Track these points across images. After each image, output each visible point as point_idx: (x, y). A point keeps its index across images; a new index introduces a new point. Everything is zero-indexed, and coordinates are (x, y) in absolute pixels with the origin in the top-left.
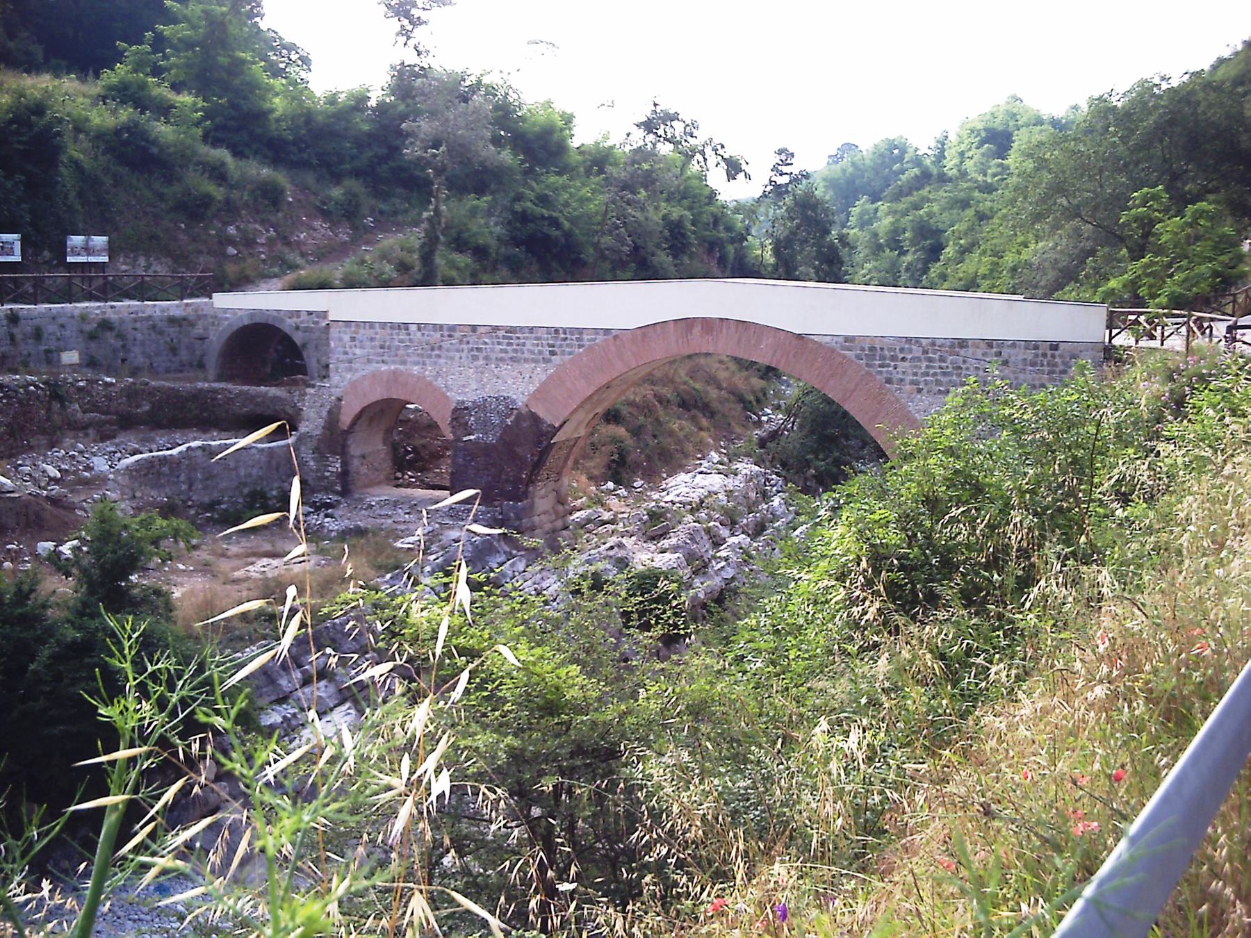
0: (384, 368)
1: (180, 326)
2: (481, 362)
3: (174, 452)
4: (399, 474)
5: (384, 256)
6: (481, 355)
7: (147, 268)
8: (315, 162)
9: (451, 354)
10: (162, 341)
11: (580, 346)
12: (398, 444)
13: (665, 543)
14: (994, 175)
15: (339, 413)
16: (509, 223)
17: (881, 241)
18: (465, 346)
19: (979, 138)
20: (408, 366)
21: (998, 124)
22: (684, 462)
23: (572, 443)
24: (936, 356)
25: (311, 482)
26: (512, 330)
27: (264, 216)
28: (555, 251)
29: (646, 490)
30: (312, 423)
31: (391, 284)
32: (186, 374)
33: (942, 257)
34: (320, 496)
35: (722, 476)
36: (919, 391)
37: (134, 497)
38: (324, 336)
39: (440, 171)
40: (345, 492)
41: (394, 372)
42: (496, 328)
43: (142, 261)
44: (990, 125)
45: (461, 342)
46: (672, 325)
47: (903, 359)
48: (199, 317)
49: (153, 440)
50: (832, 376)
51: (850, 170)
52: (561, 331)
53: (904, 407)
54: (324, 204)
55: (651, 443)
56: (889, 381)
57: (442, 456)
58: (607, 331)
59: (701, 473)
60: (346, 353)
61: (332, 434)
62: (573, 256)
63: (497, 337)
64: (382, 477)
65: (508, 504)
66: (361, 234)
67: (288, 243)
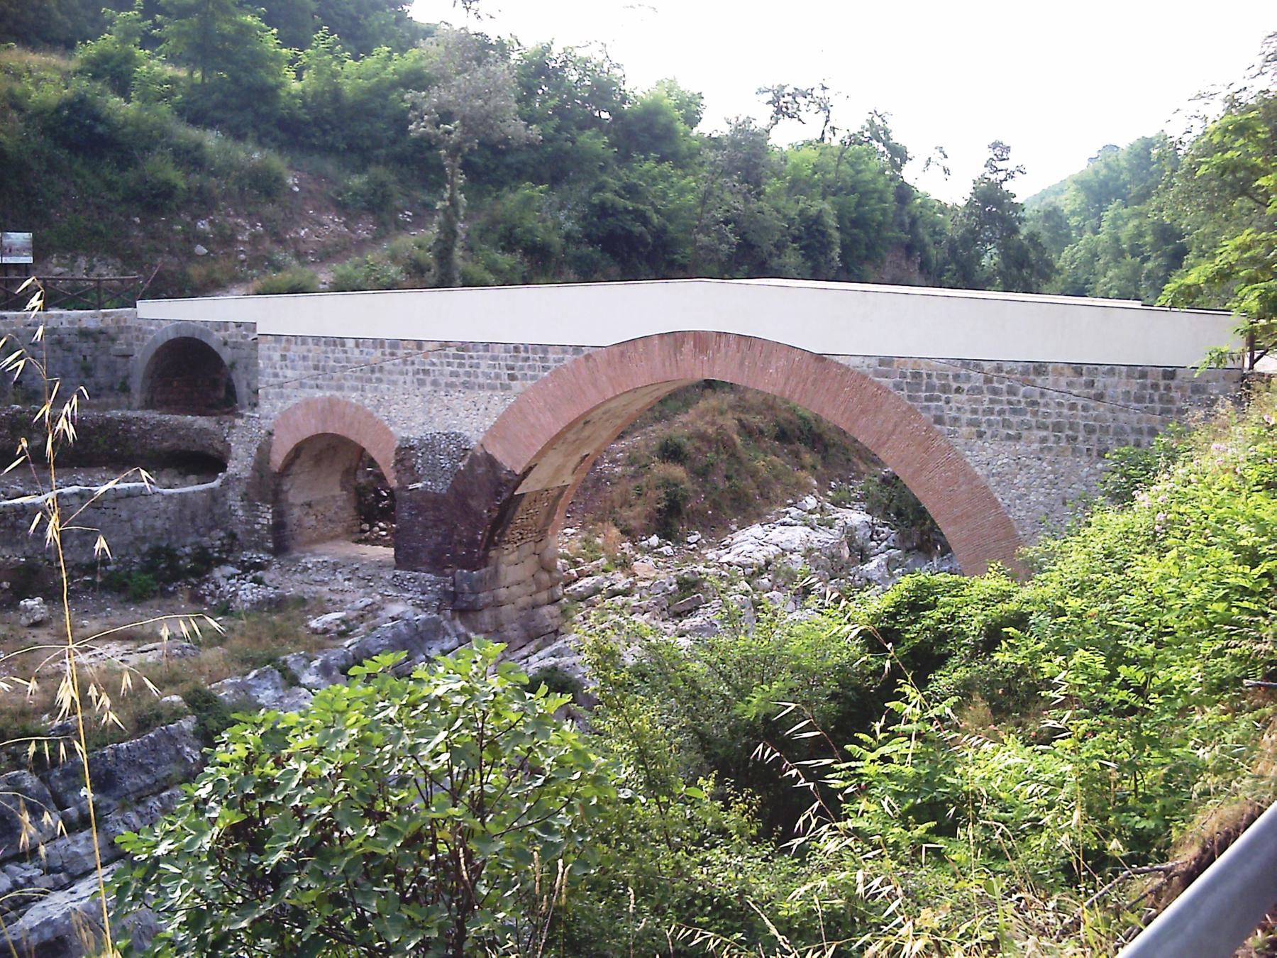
0: (319, 394)
1: (97, 341)
2: (429, 388)
4: (366, 526)
5: (394, 258)
6: (429, 379)
7: (91, 268)
8: (342, 146)
9: (394, 377)
10: (70, 359)
11: (545, 368)
12: (364, 488)
13: (687, 623)
15: (269, 451)
16: (585, 218)
17: (1125, 246)
18: (410, 368)
20: (346, 393)
23: (556, 493)
24: (1003, 387)
26: (464, 347)
27: (252, 209)
29: (703, 546)
30: (240, 464)
34: (249, 554)
35: (808, 529)
36: (980, 435)
42: (445, 344)
43: (82, 262)
45: (405, 362)
47: (958, 390)
48: (121, 330)
50: (863, 412)
51: (1104, 172)
52: (522, 348)
53: (961, 457)
54: (340, 194)
55: (721, 486)
56: (939, 420)
58: (577, 349)
59: (783, 524)
60: (276, 375)
61: (262, 477)
63: (447, 356)
64: (339, 530)
65: (461, 573)
67: (281, 241)
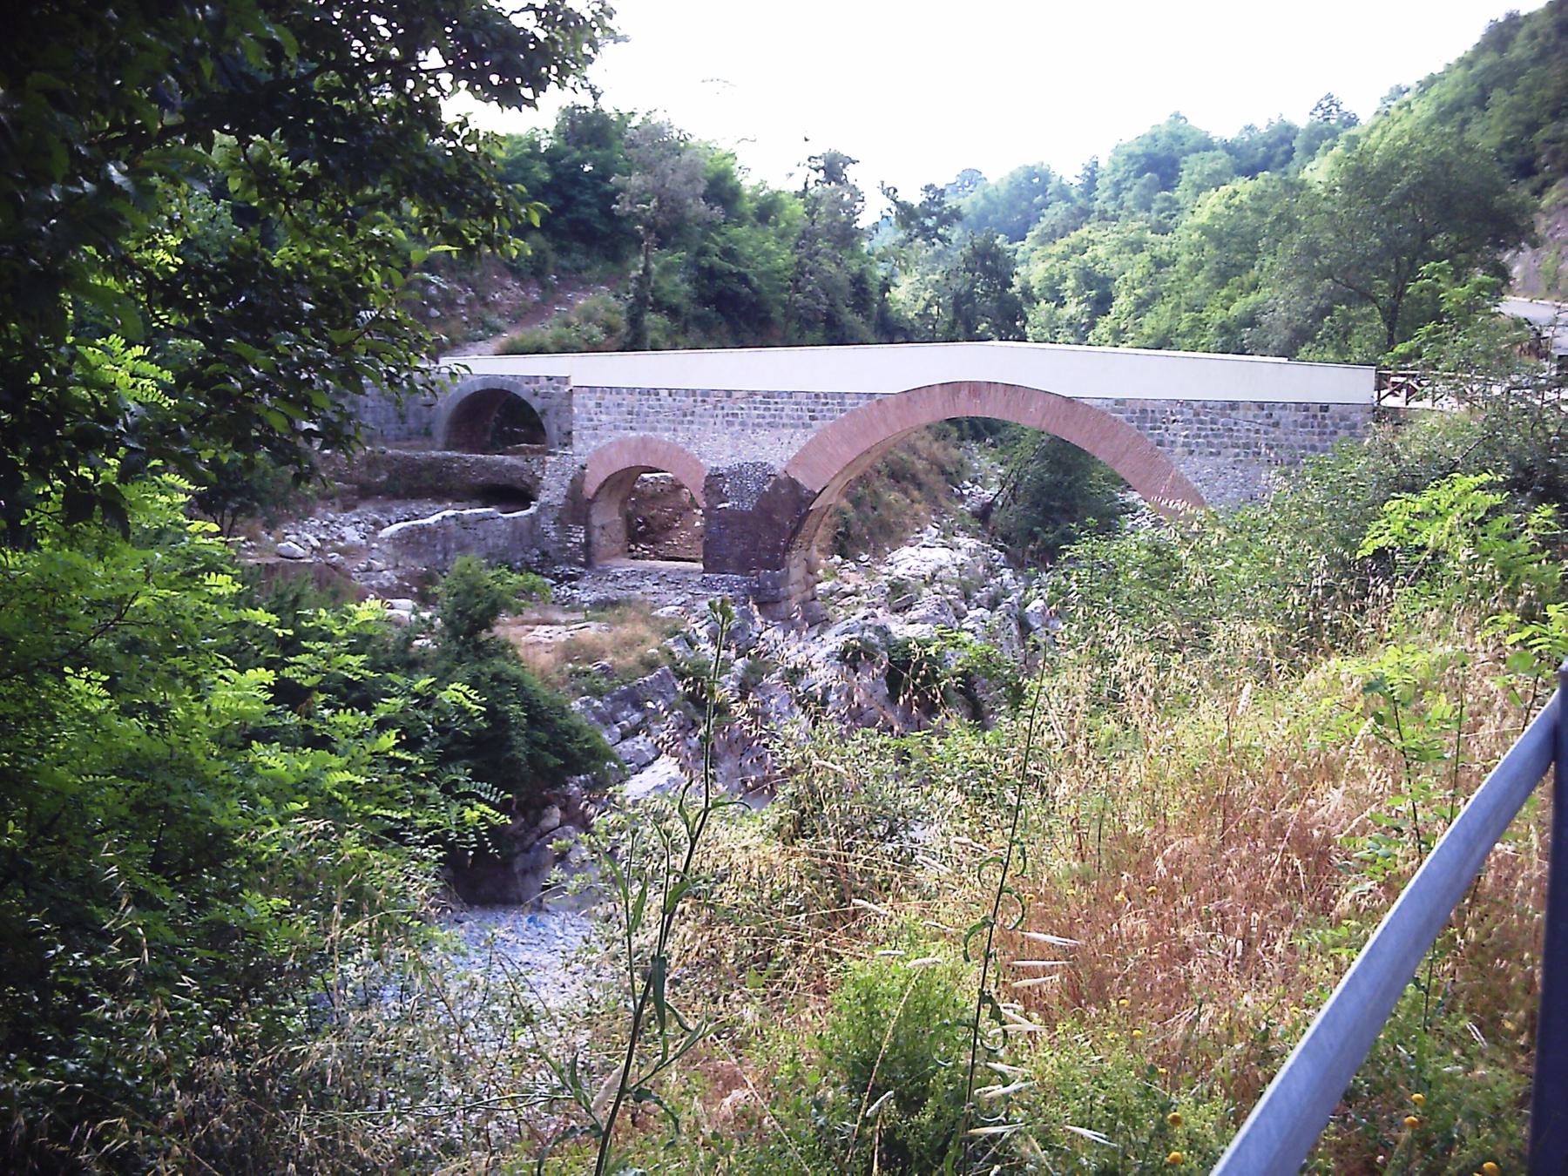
0: (632, 434)
2: (737, 428)
3: (431, 520)
4: (633, 547)
9: (705, 420)
13: (913, 615)
14: (1161, 211)
15: (583, 481)
16: (697, 281)
18: (719, 412)
19: (1136, 166)
20: (658, 433)
21: (1158, 150)
22: (904, 535)
25: (551, 553)
26: (769, 395)
28: (743, 309)
30: (552, 491)
31: (602, 348)
32: (413, 443)
33: (1112, 310)
34: (562, 568)
36: (1191, 453)
37: (397, 566)
38: (566, 402)
39: (649, 228)
40: (588, 564)
41: (643, 439)
42: (752, 394)
44: (1153, 150)
45: (715, 407)
46: (938, 389)
49: (389, 511)
51: (982, 203)
56: (1160, 443)
57: (670, 528)
59: (924, 546)
62: (762, 315)
63: (754, 402)
66: (551, 295)
67: (486, 305)
